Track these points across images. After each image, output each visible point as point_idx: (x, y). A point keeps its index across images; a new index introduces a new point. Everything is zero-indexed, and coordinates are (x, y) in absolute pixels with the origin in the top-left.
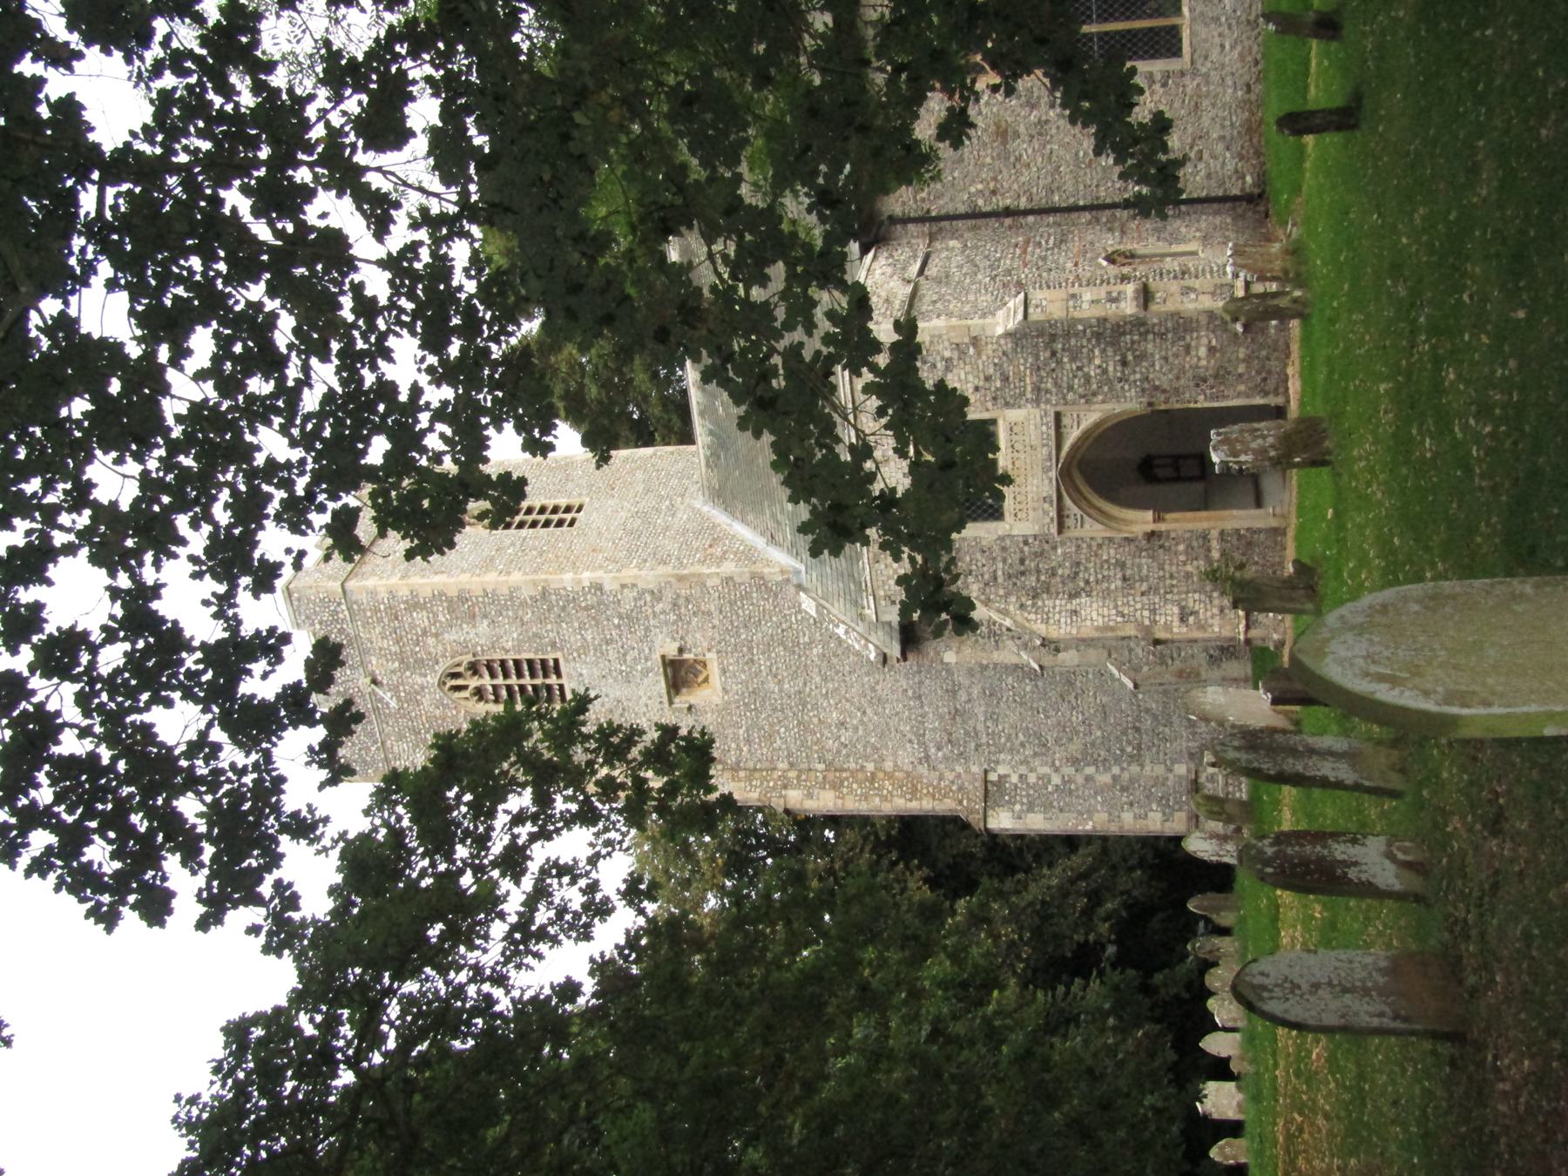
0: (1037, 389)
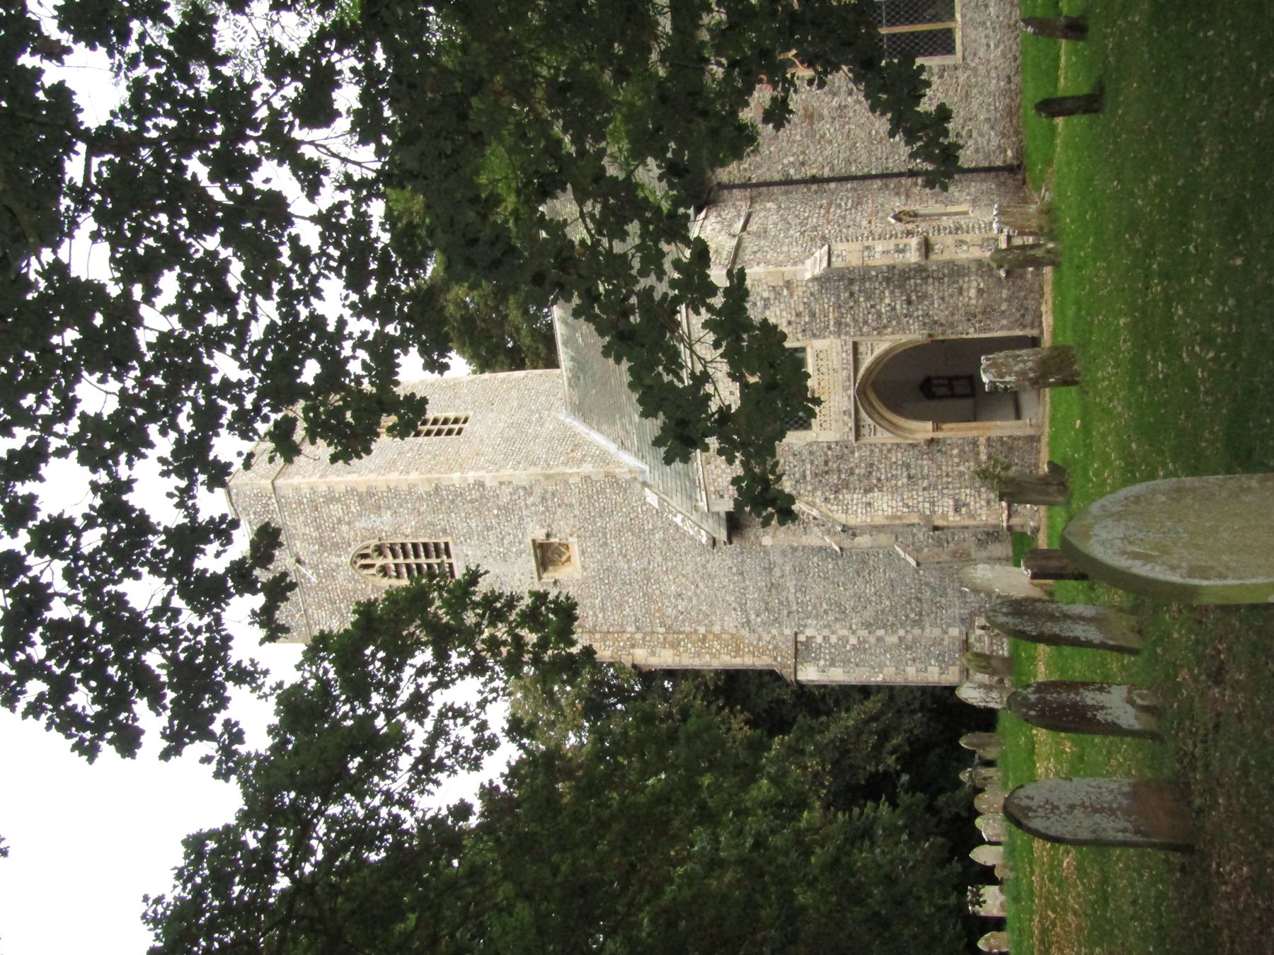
0: (838, 324)
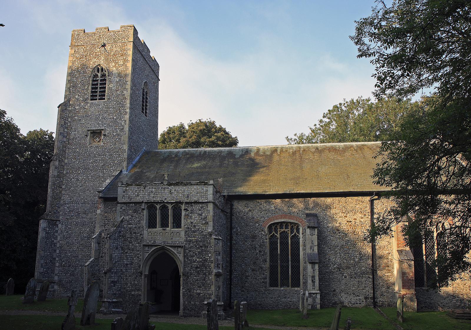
0: (190, 241)
